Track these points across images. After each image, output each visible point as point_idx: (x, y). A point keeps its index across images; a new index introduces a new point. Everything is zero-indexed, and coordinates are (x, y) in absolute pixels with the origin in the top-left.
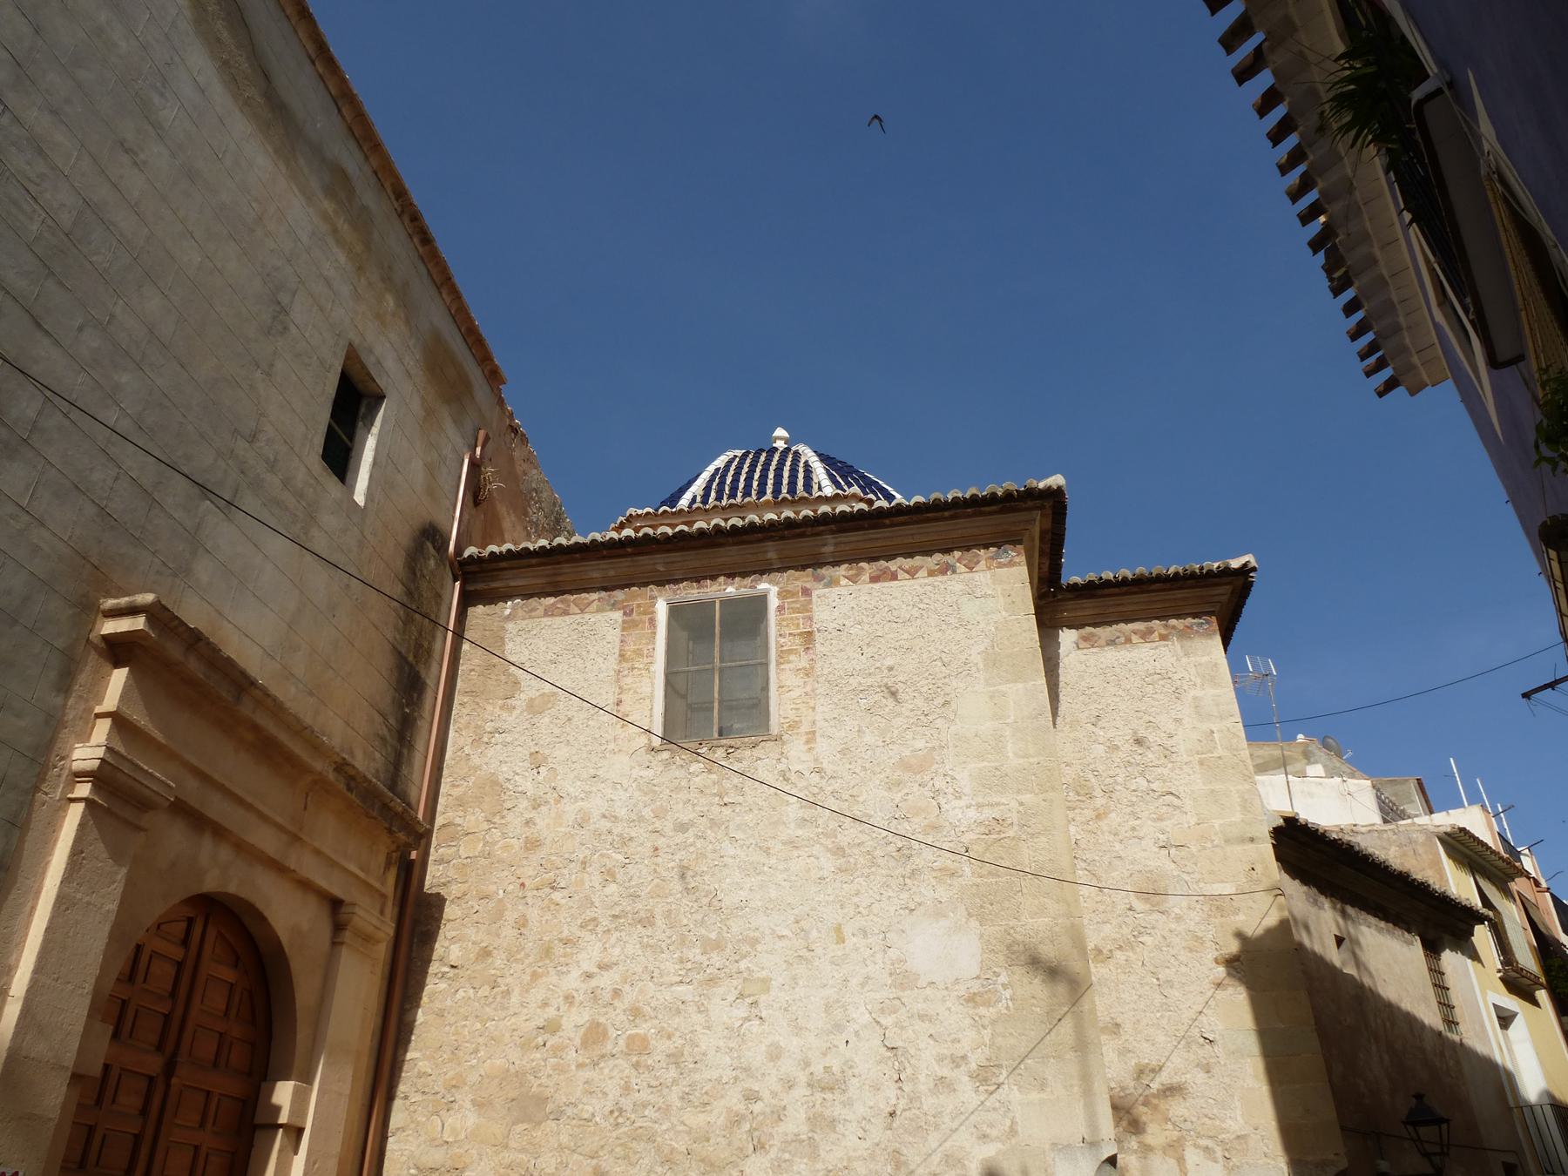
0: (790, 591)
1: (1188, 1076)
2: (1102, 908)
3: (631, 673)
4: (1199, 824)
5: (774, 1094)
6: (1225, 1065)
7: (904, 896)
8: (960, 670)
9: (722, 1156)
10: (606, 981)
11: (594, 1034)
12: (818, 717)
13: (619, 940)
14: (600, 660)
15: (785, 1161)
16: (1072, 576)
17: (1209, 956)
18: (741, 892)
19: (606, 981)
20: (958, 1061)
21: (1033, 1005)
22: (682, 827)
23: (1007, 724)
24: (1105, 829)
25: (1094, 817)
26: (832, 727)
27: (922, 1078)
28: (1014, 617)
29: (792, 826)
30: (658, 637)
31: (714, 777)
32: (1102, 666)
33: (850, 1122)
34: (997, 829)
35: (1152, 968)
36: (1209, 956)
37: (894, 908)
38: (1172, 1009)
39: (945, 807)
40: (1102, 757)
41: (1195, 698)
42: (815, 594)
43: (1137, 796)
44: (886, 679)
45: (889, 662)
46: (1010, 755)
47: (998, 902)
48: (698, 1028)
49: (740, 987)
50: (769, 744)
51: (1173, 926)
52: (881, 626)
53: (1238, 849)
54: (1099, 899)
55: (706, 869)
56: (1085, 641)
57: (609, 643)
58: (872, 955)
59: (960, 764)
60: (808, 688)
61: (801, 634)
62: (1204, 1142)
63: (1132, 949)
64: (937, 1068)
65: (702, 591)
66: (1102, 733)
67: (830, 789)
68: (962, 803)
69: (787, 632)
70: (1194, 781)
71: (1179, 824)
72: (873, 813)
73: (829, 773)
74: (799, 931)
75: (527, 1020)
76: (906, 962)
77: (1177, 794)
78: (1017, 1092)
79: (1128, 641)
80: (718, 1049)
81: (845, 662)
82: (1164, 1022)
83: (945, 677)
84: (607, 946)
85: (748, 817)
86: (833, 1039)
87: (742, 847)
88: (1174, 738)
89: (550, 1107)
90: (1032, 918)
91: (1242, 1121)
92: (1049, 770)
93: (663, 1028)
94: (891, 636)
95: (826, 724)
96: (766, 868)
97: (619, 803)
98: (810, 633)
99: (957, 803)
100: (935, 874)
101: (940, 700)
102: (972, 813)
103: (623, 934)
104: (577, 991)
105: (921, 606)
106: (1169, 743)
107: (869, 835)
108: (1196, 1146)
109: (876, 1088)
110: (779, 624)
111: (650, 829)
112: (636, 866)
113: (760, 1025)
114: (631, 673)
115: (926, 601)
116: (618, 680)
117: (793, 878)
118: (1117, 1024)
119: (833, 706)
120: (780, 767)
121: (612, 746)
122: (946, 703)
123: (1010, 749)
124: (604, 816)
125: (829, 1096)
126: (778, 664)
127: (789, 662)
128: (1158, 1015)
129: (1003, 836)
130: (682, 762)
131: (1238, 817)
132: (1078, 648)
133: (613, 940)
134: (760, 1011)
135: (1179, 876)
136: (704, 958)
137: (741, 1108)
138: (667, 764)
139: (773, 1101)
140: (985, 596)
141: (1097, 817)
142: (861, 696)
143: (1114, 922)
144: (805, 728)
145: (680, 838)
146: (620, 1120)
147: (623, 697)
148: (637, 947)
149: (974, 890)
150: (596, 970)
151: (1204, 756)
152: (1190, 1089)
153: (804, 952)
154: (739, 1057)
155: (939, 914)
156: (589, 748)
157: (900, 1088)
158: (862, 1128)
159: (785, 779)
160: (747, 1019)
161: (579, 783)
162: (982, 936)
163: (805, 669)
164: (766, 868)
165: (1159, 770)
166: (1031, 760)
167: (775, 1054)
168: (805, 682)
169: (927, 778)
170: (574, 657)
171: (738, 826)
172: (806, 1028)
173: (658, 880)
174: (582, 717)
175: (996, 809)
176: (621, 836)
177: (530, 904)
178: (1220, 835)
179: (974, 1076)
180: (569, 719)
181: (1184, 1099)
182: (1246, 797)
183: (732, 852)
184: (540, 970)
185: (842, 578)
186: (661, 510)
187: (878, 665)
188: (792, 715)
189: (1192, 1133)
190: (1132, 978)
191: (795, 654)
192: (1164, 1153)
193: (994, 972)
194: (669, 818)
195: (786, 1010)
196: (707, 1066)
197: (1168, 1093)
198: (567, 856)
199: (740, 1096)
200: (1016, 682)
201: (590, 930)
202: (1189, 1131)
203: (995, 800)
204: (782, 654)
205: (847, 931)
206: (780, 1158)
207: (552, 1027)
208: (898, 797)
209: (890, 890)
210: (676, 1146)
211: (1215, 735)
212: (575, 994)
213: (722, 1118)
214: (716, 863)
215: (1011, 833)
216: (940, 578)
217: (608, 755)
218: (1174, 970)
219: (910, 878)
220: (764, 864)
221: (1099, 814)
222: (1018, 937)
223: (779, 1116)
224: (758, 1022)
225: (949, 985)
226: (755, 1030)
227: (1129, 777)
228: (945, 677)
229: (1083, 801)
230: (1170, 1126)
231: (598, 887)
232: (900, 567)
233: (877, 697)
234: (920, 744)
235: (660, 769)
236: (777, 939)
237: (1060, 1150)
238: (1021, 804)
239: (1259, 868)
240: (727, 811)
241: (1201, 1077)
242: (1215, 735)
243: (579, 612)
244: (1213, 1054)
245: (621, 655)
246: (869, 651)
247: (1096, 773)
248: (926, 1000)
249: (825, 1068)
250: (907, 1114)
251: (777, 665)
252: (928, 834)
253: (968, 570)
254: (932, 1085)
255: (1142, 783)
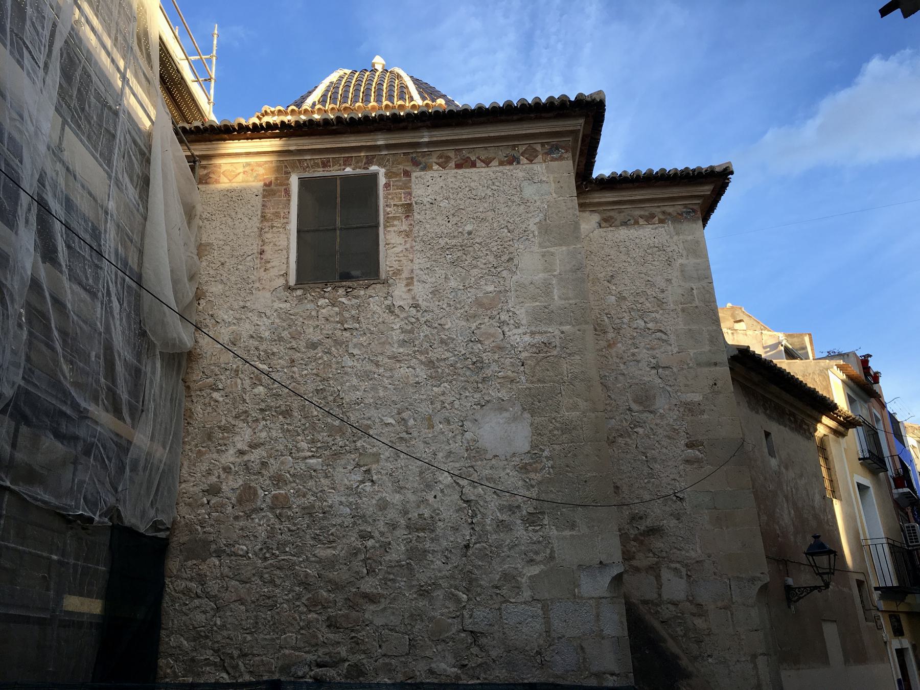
0: (394, 173)
1: (665, 522)
2: (609, 409)
3: (271, 230)
4: (679, 353)
5: (382, 534)
6: (690, 515)
7: (477, 395)
8: (521, 236)
9: (344, 578)
10: (255, 456)
11: (247, 494)
12: (416, 267)
13: (265, 426)
14: (246, 220)
15: (390, 580)
16: (603, 167)
17: (683, 442)
18: (358, 393)
19: (255, 456)
20: (513, 509)
21: (567, 471)
22: (313, 346)
23: (554, 276)
24: (614, 354)
25: (606, 346)
26: (425, 274)
27: (488, 521)
28: (561, 198)
29: (396, 345)
30: (292, 203)
31: (337, 309)
32: (616, 240)
33: (436, 552)
34: (545, 350)
35: (642, 450)
36: (683, 442)
37: (470, 404)
38: (655, 477)
39: (508, 334)
40: (613, 305)
41: (681, 265)
42: (414, 175)
43: (637, 332)
44: (466, 241)
45: (469, 228)
46: (556, 297)
47: (544, 401)
48: (326, 488)
49: (357, 459)
50: (379, 286)
51: (658, 421)
52: (463, 201)
53: (705, 370)
54: (607, 402)
55: (331, 376)
56: (605, 222)
57: (253, 206)
58: (454, 437)
59: (520, 303)
60: (408, 246)
61: (402, 205)
62: (673, 565)
63: (629, 436)
64: (498, 514)
65: (326, 169)
66: (614, 288)
67: (424, 319)
68: (520, 331)
69: (392, 203)
70: (678, 323)
71: (665, 352)
72: (455, 337)
73: (424, 308)
74: (400, 420)
75: (194, 486)
76: (478, 441)
77: (665, 331)
78: (555, 531)
79: (637, 223)
80: (341, 503)
81: (436, 227)
82: (650, 485)
83: (510, 241)
84: (256, 431)
85: (362, 339)
86: (425, 496)
87: (358, 360)
88: (665, 293)
89: (213, 547)
90: (568, 412)
91: (699, 551)
92: (583, 309)
93: (299, 489)
94: (471, 209)
95: (422, 272)
96: (376, 376)
97: (263, 328)
98: (410, 205)
99: (516, 331)
100: (499, 381)
101: (505, 257)
102: (527, 338)
103: (268, 422)
104: (234, 464)
105: (493, 187)
106: (661, 296)
107: (451, 352)
108: (668, 568)
109: (456, 529)
110: (386, 197)
111: (288, 346)
112: (278, 374)
113: (372, 486)
114: (271, 230)
115: (497, 184)
116: (260, 235)
117: (397, 383)
118: (617, 487)
119: (427, 260)
120: (386, 302)
121: (257, 285)
122: (510, 260)
123: (556, 294)
124: (252, 337)
125: (421, 534)
126: (385, 227)
127: (393, 226)
128: (646, 481)
129: (549, 354)
130: (311, 298)
131: (707, 348)
132: (600, 227)
133: (260, 427)
134: (372, 477)
135: (663, 387)
136: (330, 439)
137: (358, 544)
138: (300, 300)
139: (381, 538)
140: (541, 182)
141: (608, 346)
142: (447, 252)
143: (618, 418)
144: (405, 275)
145: (312, 353)
146: (268, 555)
147: (266, 248)
148: (280, 431)
149: (527, 392)
150: (247, 448)
151: (685, 306)
152: (666, 531)
153: (404, 435)
154: (357, 509)
155: (502, 409)
156: (239, 286)
157: (473, 528)
158: (445, 556)
159: (390, 312)
160: (362, 482)
161: (231, 312)
162: (532, 424)
163: (405, 231)
164: (376, 376)
165: (653, 315)
166: (571, 302)
167: (383, 505)
168: (406, 241)
169: (495, 313)
170: (225, 216)
171: (355, 345)
172: (405, 487)
173: (295, 384)
174: (233, 262)
175: (544, 336)
176: (265, 351)
177: (195, 401)
178: (693, 360)
179: (526, 519)
180: (223, 264)
181: (662, 537)
182: (713, 335)
183: (350, 363)
184: (204, 449)
185: (434, 164)
186: (290, 108)
187: (460, 230)
188: (396, 265)
189: (666, 559)
190: (628, 456)
191: (398, 220)
192: (647, 572)
193: (541, 449)
194: (302, 338)
195: (391, 475)
196: (333, 515)
197: (650, 533)
198: (223, 366)
199: (357, 536)
200: (561, 245)
201: (243, 420)
202: (664, 558)
203: (544, 329)
204: (388, 219)
205: (436, 420)
206: (386, 578)
207: (214, 490)
208: (474, 326)
209: (467, 392)
210: (310, 572)
211: (694, 291)
212: (232, 466)
213: (343, 552)
214: (339, 371)
215: (555, 353)
216: (508, 167)
217: (254, 291)
218: (657, 451)
219: (481, 383)
220: (374, 373)
221: (610, 344)
222: (558, 425)
223: (386, 549)
224: (370, 484)
225: (508, 457)
226: (368, 489)
227: (632, 319)
228: (510, 241)
229: (599, 335)
230: (651, 555)
231: (248, 389)
232: (478, 158)
233: (459, 254)
234: (491, 288)
235: (296, 303)
236: (384, 426)
237: (584, 570)
238: (562, 332)
239: (719, 384)
240: (347, 334)
241: (673, 522)
242: (694, 291)
243: (228, 181)
244: (682, 507)
245: (262, 216)
246: (454, 220)
247: (609, 316)
248: (491, 468)
249: (419, 514)
250: (478, 546)
251: (385, 228)
252: (495, 353)
253: (529, 162)
254: (495, 526)
255: (641, 323)
